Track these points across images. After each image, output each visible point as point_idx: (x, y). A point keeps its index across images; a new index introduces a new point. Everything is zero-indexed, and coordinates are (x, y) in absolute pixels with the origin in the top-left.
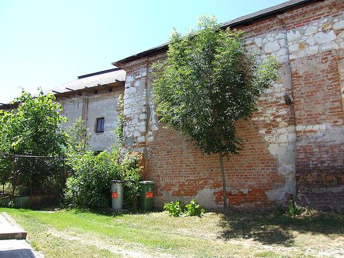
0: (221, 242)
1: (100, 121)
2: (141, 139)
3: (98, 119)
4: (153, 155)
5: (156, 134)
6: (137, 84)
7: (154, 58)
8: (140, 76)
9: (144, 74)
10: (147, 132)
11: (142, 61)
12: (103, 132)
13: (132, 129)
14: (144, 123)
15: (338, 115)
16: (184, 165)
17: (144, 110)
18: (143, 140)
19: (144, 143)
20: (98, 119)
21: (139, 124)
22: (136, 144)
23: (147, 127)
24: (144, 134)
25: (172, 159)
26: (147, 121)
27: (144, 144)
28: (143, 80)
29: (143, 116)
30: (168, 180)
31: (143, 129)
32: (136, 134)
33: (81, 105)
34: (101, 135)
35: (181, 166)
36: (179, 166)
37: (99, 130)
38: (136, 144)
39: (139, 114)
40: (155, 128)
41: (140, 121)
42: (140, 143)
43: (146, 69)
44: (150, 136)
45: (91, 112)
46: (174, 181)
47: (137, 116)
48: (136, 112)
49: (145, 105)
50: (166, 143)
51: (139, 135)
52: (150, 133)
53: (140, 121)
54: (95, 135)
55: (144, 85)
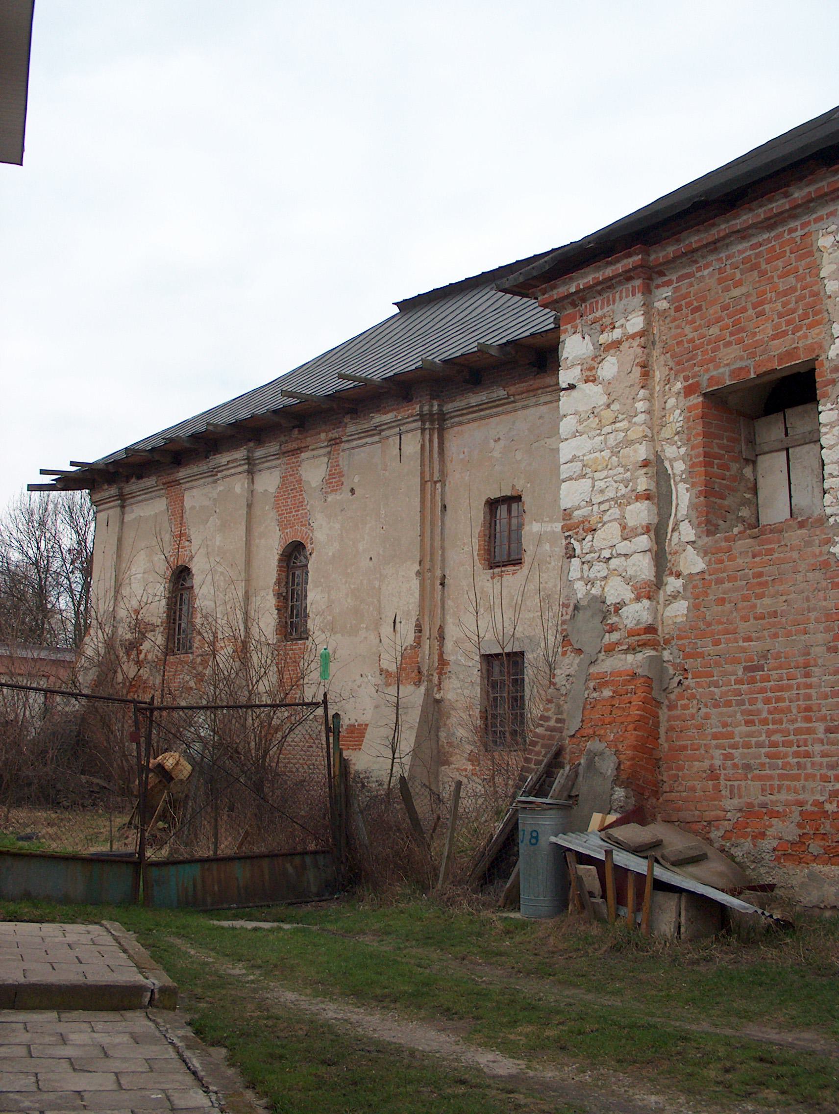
0: (661, 837)
1: (502, 506)
2: (636, 613)
3: (493, 505)
4: (690, 682)
5: (698, 588)
6: (609, 368)
7: (671, 250)
8: (617, 334)
9: (636, 323)
10: (659, 584)
11: (620, 267)
12: (518, 562)
13: (599, 570)
14: (644, 541)
15: (765, 584)
16: (820, 727)
17: (643, 484)
18: (646, 618)
19: (651, 629)
20: (493, 505)
21: (623, 547)
22: (615, 636)
23: (661, 560)
24: (649, 592)
25: (767, 701)
26: (658, 531)
27: (648, 636)
28: (632, 351)
29: (640, 513)
30: (753, 792)
31: (643, 567)
32: (616, 591)
33: (412, 444)
34: (513, 580)
35: (809, 731)
36: (797, 732)
37: (501, 554)
38: (615, 636)
39: (620, 502)
40: (693, 562)
41: (627, 534)
42: (631, 633)
43: (639, 299)
44: (675, 597)
45: (457, 476)
46: (783, 796)
47: (615, 512)
48: (611, 494)
49: (646, 464)
50: (743, 626)
51: (628, 594)
52: (673, 584)
53: (627, 534)
54: (484, 577)
55: (637, 371)
